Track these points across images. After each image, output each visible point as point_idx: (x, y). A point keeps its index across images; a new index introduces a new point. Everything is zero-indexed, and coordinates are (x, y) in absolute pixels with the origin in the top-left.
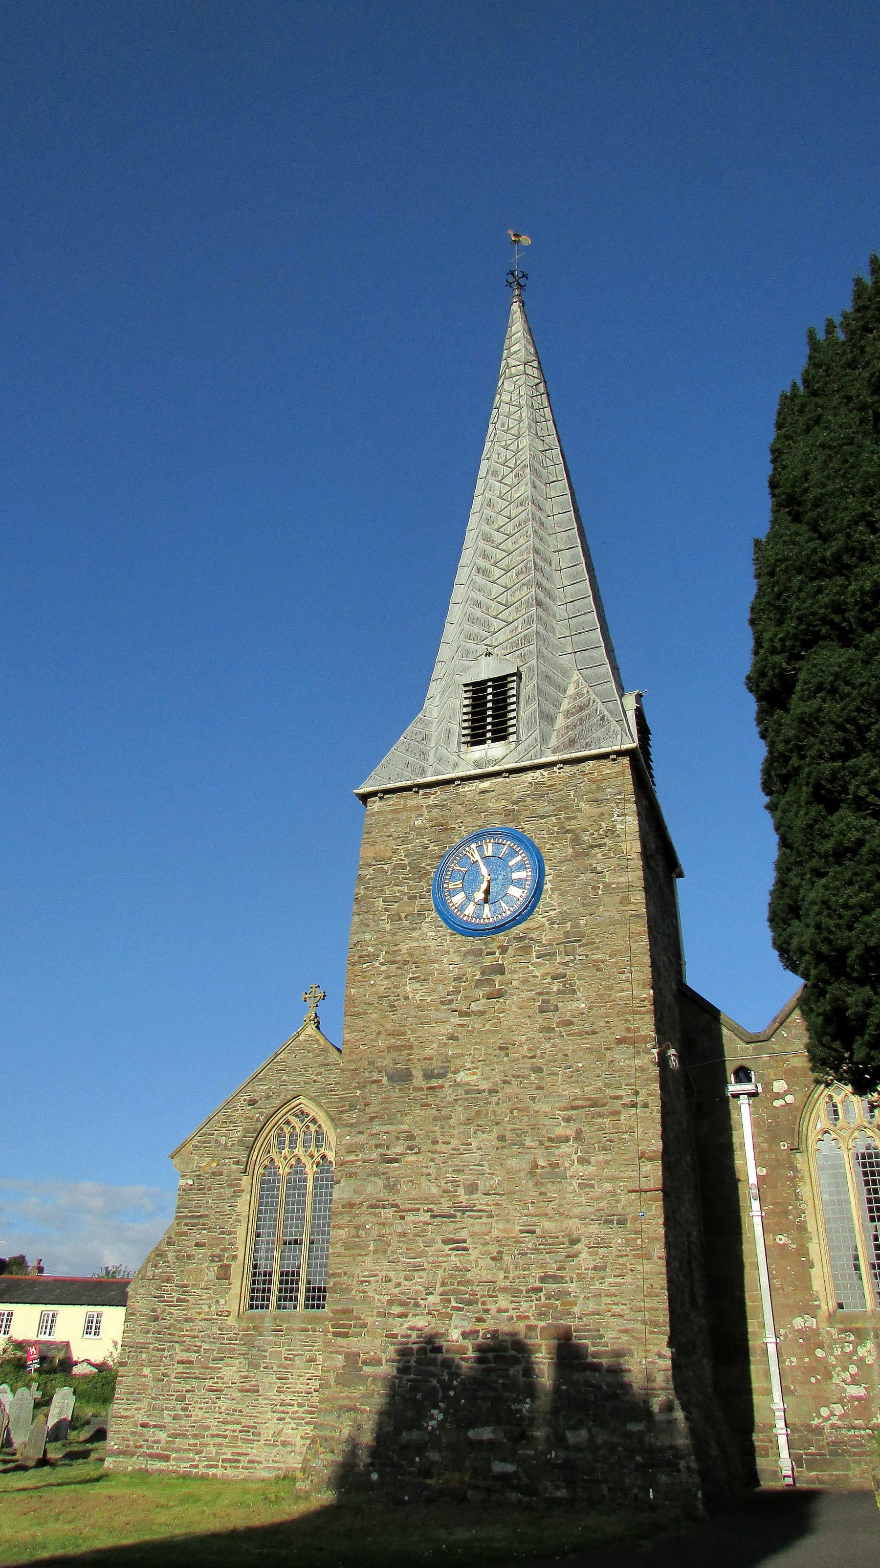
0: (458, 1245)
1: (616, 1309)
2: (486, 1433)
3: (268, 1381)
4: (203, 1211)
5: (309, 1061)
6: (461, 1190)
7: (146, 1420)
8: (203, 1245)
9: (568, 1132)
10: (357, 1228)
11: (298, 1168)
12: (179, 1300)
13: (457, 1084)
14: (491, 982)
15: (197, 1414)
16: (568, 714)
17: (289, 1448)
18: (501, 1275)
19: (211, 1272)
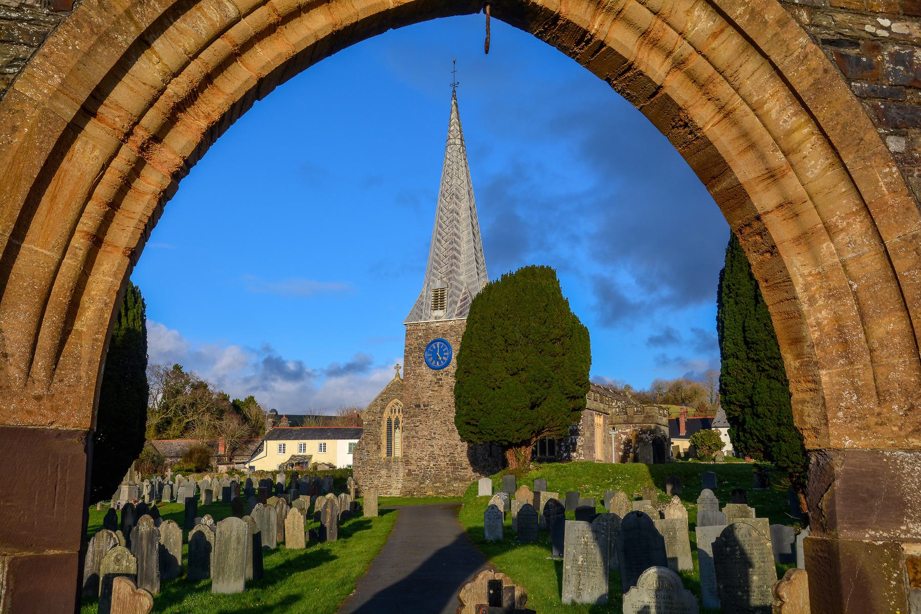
0: (432, 446)
2: (438, 485)
3: (393, 474)
11: (397, 419)
16: (461, 301)
19: (375, 447)
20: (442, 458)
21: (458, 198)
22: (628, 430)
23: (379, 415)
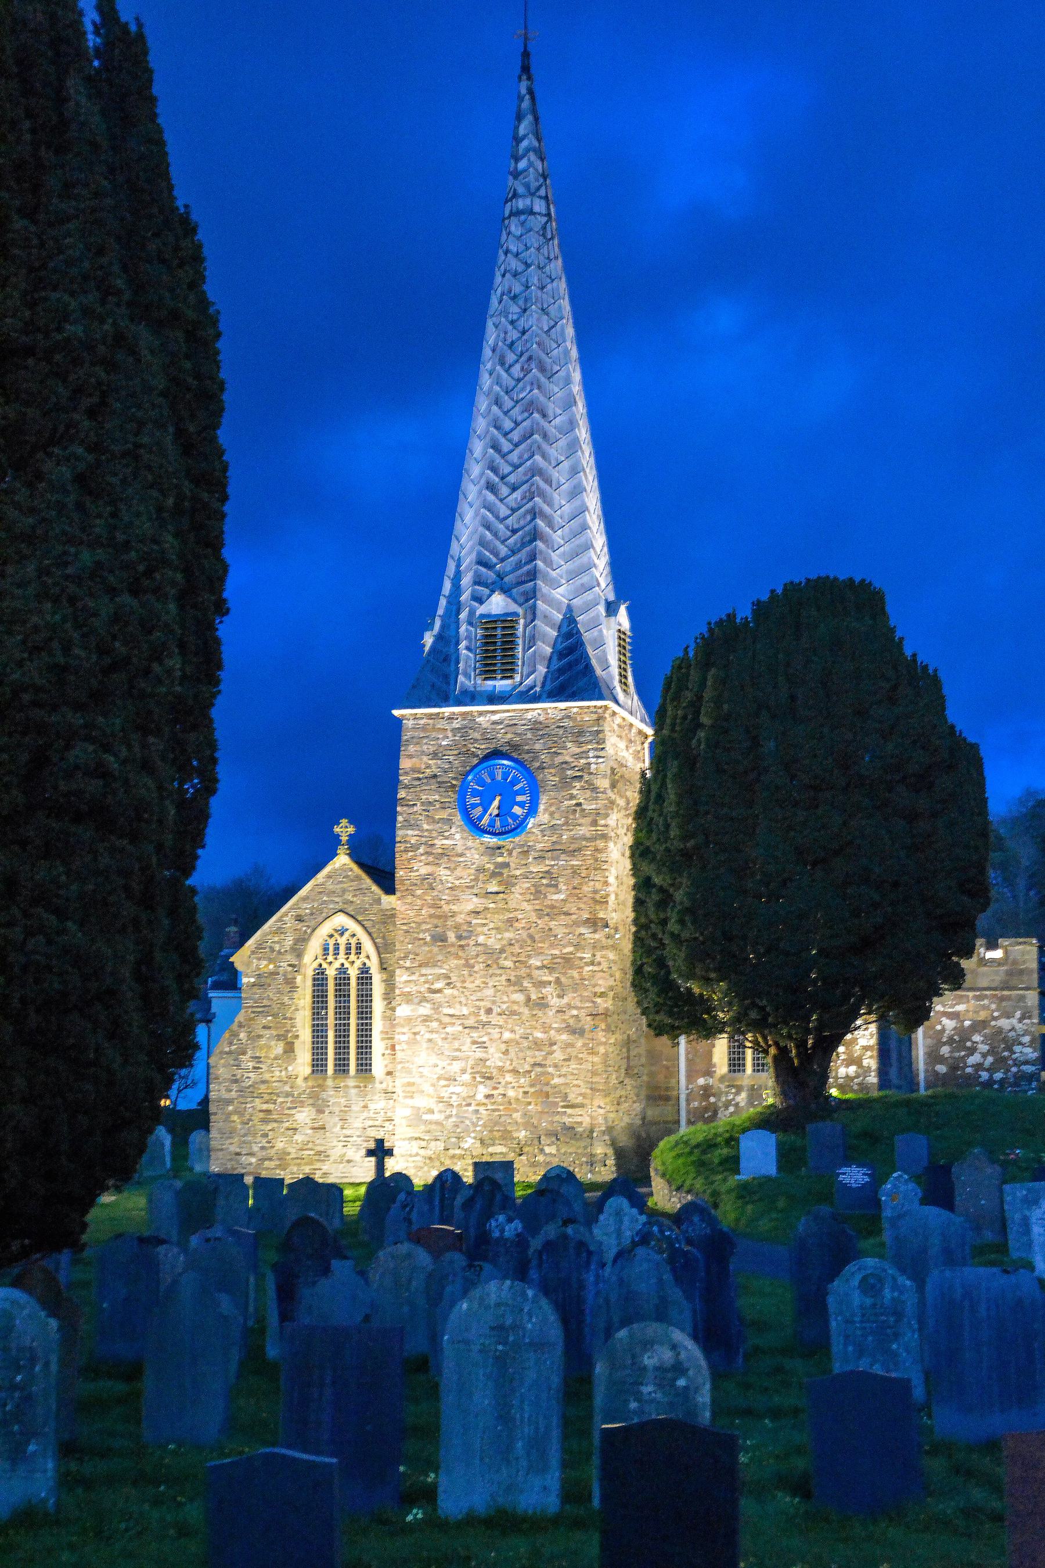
0: (482, 1045)
1: (575, 1082)
3: (332, 1122)
4: (266, 1002)
5: (345, 885)
6: (482, 1012)
7: (238, 1150)
8: (270, 1028)
9: (551, 979)
10: (415, 1034)
11: (365, 970)
12: (254, 1068)
13: (477, 944)
14: (501, 874)
15: (279, 1145)
17: (351, 1164)
18: (508, 1063)
19: (279, 1048)
20: (509, 1078)
21: (542, 369)
22: (961, 1008)
23: (291, 958)
